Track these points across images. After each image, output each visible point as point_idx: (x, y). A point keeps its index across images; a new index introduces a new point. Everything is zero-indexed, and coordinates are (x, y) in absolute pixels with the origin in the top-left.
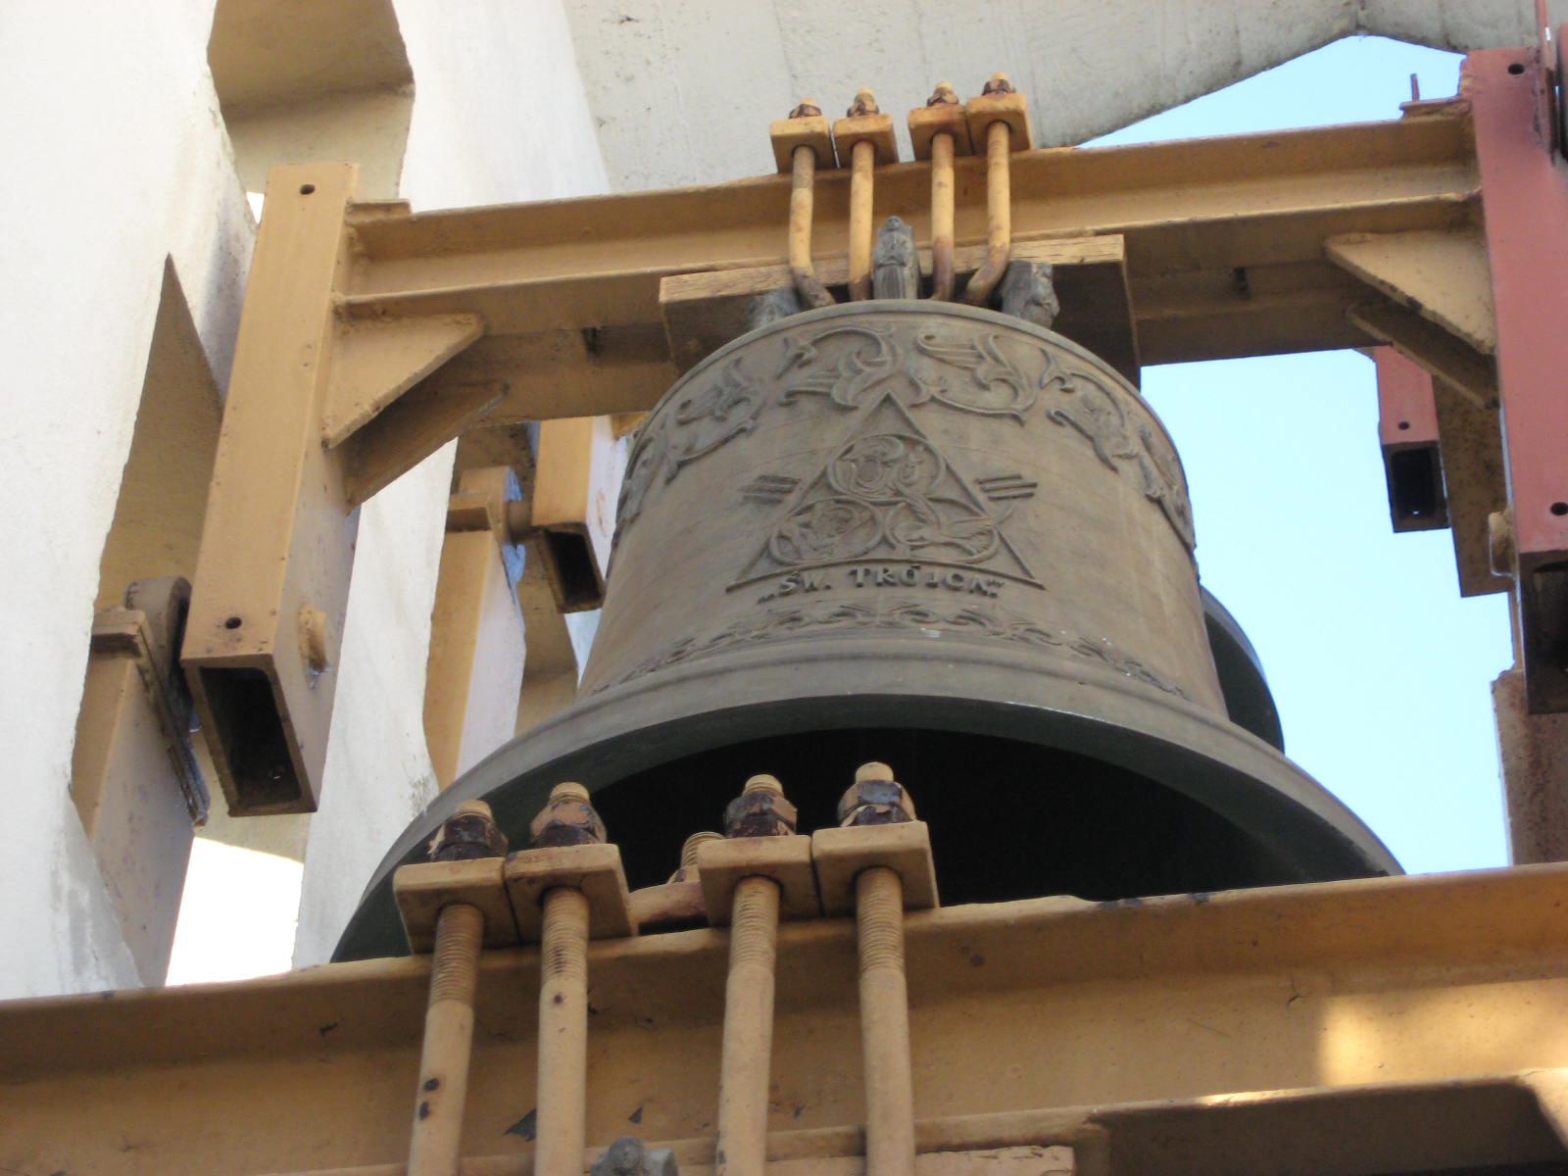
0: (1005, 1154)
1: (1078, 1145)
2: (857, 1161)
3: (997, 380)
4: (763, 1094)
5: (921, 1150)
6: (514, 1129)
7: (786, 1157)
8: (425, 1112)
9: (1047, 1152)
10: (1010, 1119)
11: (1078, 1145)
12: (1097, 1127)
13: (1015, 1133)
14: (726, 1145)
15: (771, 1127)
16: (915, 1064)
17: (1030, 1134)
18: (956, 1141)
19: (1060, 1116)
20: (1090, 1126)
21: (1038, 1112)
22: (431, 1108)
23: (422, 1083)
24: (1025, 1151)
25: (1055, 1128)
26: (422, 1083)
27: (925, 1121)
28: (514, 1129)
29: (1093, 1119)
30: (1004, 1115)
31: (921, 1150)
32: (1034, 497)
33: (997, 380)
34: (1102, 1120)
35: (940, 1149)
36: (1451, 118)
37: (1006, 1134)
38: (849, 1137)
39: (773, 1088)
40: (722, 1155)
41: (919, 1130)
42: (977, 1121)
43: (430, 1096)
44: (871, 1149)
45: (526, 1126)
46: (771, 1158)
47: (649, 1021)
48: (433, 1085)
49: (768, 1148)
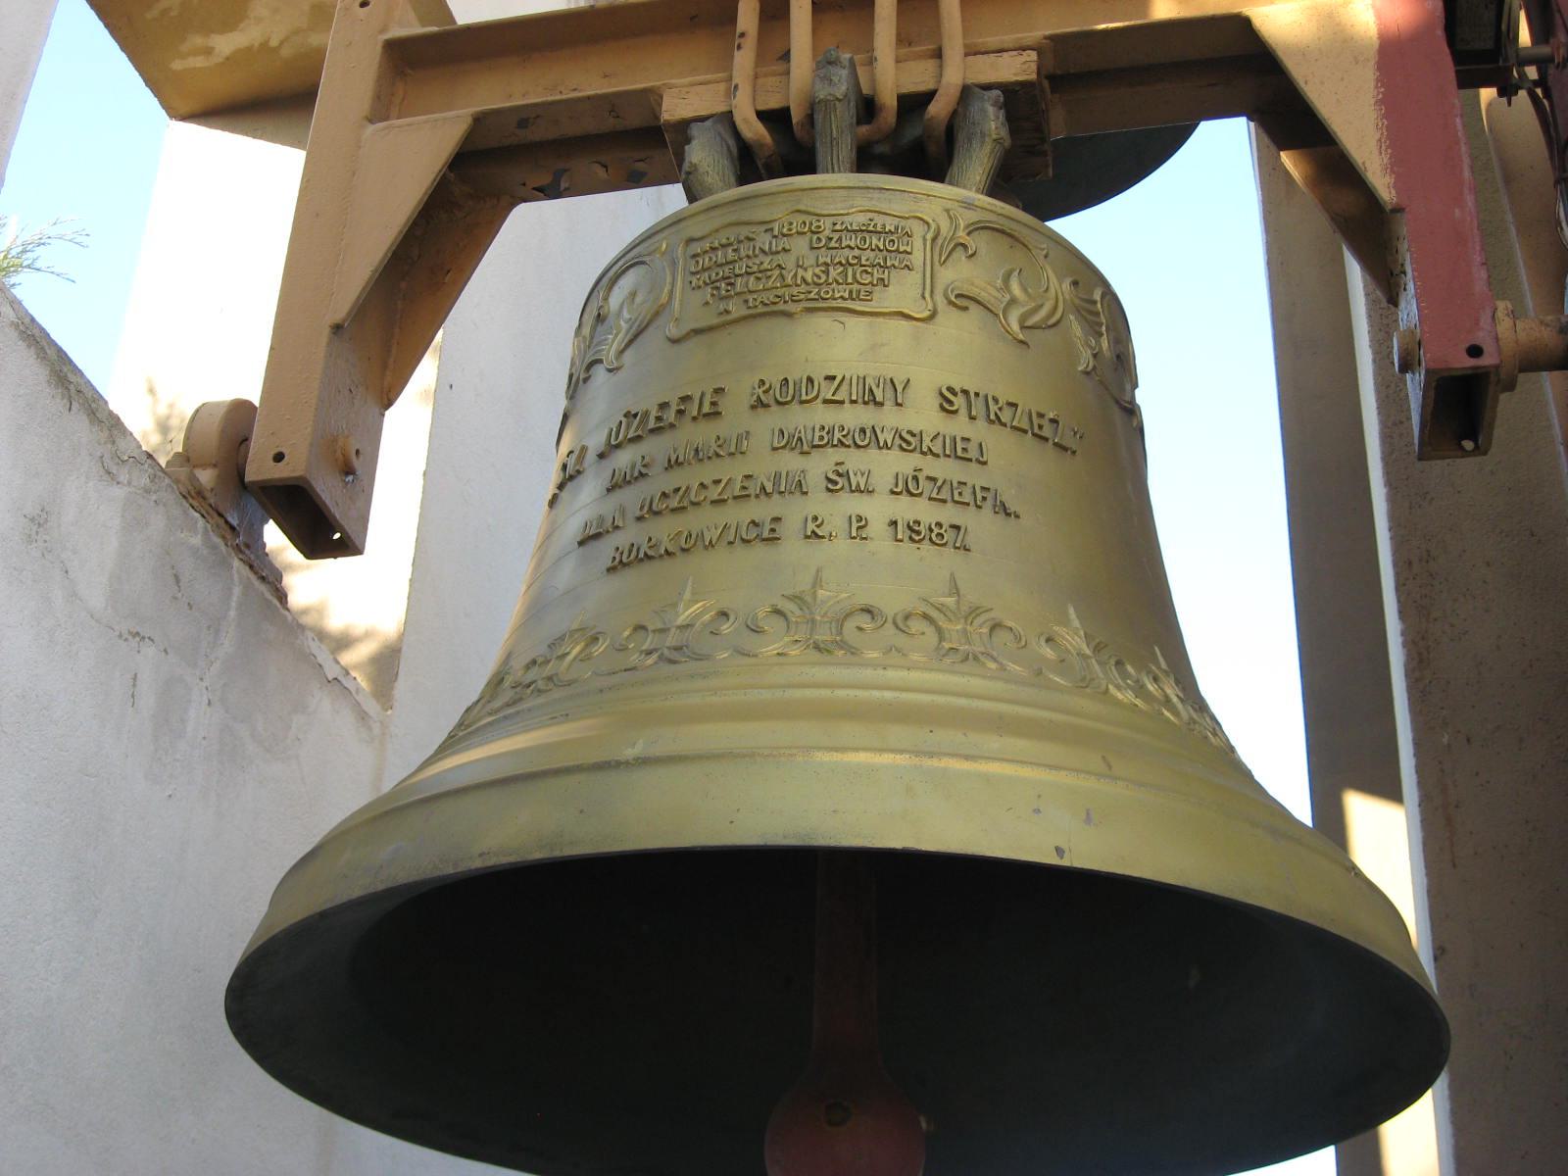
0: (1005, 55)
1: (1039, 49)
2: (938, 61)
3: (792, 212)
4: (894, 38)
5: (967, 55)
6: (781, 58)
7: (906, 60)
8: (739, 47)
9: (1024, 53)
10: (1008, 39)
11: (1039, 49)
12: (1048, 41)
13: (1011, 46)
14: (878, 53)
15: (897, 49)
16: (964, 20)
17: (1017, 46)
18: (983, 50)
19: (1030, 37)
20: (1044, 41)
21: (1020, 35)
22: (742, 45)
23: (737, 34)
24: (1015, 53)
25: (1028, 42)
26: (737, 34)
27: (966, 42)
28: (781, 58)
29: (1046, 38)
30: (1006, 38)
31: (967, 55)
32: (811, 375)
33: (792, 212)
34: (1051, 38)
35: (976, 54)
36: (1125, 700)
37: (1006, 46)
38: (934, 50)
39: (898, 35)
40: (876, 58)
41: (966, 46)
42: (992, 41)
43: (742, 40)
44: (944, 57)
45: (786, 56)
46: (898, 61)
47: (841, 7)
48: (742, 35)
49: (897, 57)
